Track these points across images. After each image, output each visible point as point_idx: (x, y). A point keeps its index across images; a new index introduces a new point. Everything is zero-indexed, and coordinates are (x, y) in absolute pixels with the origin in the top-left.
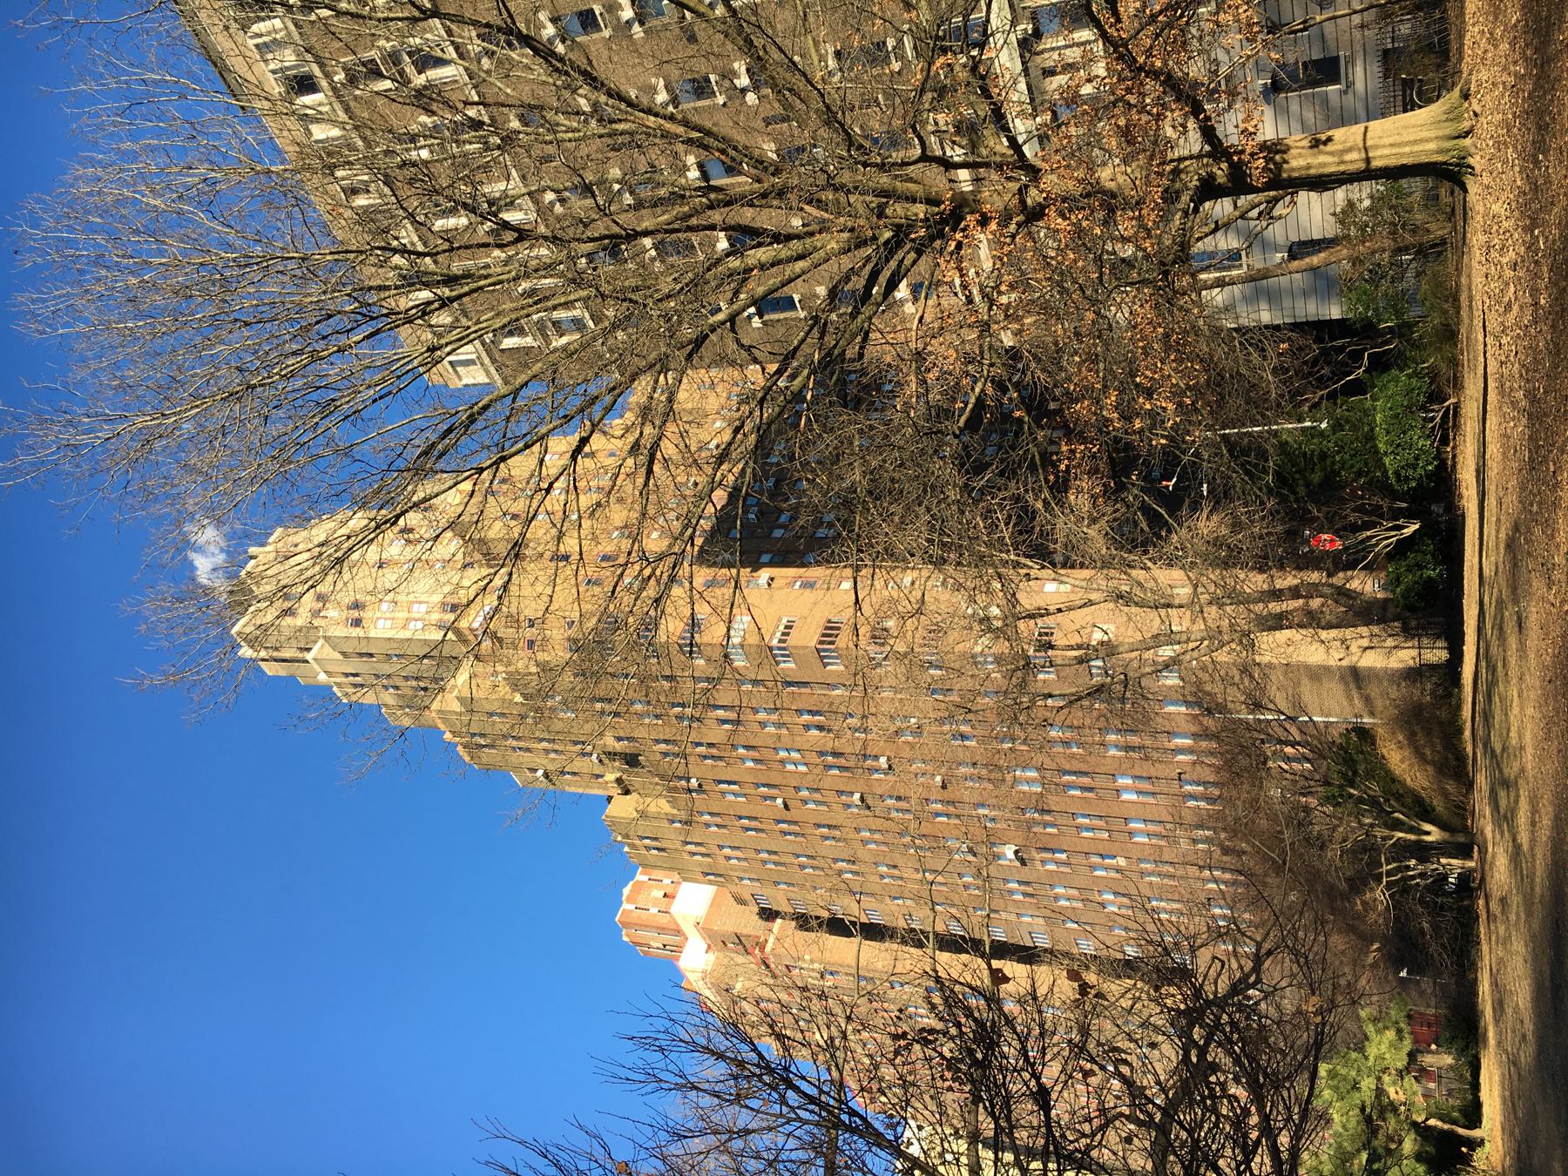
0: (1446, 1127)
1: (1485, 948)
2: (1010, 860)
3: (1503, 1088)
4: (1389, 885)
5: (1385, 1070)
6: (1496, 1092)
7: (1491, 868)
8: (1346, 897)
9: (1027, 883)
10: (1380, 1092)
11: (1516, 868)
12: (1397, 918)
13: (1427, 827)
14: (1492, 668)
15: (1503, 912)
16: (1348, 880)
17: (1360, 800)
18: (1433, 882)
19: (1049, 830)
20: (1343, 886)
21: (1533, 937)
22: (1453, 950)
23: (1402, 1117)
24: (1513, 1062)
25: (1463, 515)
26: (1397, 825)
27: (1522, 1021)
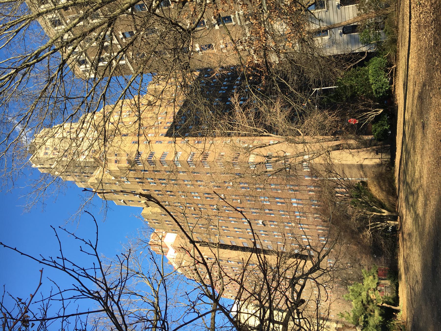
0: (388, 306)
1: (401, 249)
2: (261, 225)
3: (408, 295)
4: (371, 230)
5: (369, 289)
6: (405, 296)
7: (405, 223)
8: (357, 234)
9: (266, 231)
10: (368, 296)
11: (416, 223)
12: (374, 240)
13: (384, 211)
14: (408, 152)
15: (409, 238)
16: (358, 228)
17: (362, 203)
18: (384, 229)
19: (272, 215)
20: (356, 230)
21: (423, 248)
22: (391, 250)
23: (375, 304)
24: (412, 289)
25: (397, 107)
26: (374, 210)
27: (417, 276)
